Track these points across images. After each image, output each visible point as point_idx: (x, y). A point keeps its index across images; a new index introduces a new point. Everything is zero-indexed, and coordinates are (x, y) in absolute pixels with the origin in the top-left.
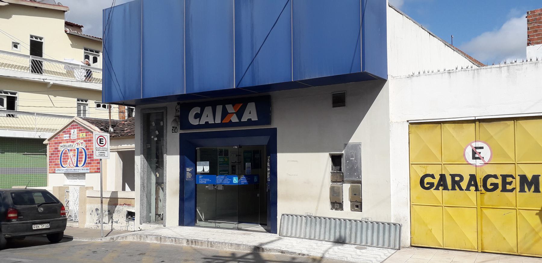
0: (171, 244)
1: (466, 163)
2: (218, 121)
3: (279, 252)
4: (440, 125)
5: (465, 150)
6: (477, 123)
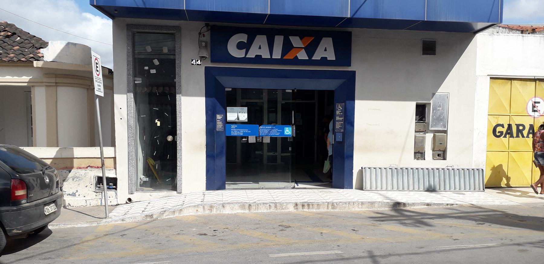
0: (269, 211)
1: (528, 115)
2: (277, 55)
3: (424, 205)
4: (510, 81)
5: (527, 104)
6: (537, 82)
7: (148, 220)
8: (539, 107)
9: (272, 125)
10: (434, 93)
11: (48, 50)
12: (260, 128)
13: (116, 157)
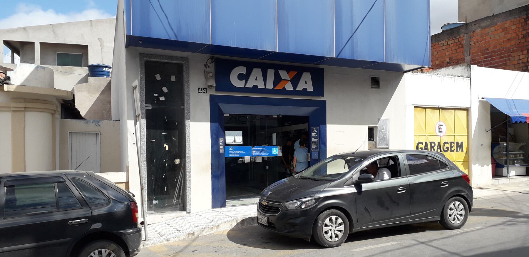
7: (190, 237)
8: (443, 129)
9: (263, 146)
10: (380, 118)
11: (15, 73)
12: (253, 149)
13: (128, 182)
